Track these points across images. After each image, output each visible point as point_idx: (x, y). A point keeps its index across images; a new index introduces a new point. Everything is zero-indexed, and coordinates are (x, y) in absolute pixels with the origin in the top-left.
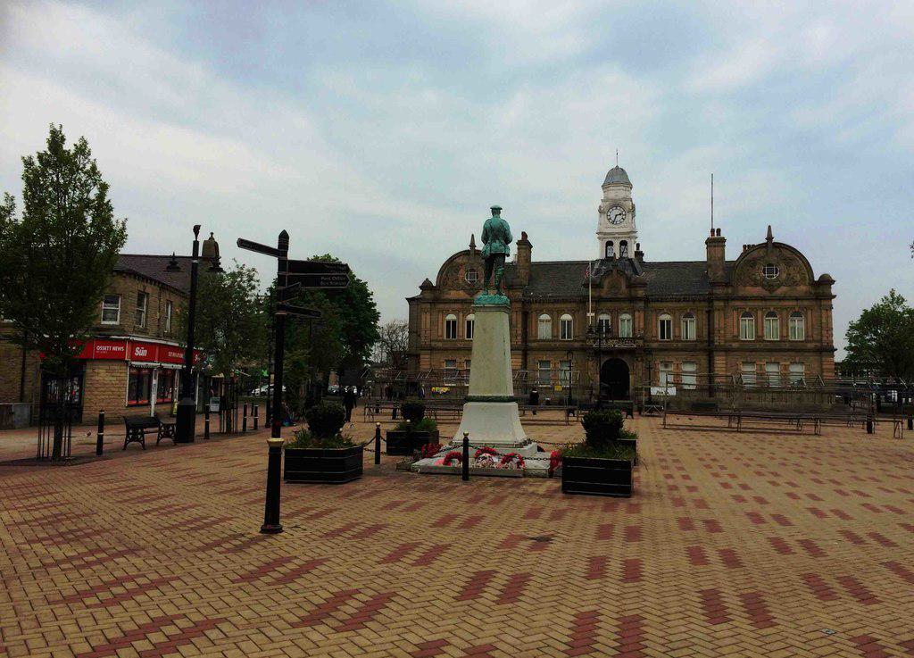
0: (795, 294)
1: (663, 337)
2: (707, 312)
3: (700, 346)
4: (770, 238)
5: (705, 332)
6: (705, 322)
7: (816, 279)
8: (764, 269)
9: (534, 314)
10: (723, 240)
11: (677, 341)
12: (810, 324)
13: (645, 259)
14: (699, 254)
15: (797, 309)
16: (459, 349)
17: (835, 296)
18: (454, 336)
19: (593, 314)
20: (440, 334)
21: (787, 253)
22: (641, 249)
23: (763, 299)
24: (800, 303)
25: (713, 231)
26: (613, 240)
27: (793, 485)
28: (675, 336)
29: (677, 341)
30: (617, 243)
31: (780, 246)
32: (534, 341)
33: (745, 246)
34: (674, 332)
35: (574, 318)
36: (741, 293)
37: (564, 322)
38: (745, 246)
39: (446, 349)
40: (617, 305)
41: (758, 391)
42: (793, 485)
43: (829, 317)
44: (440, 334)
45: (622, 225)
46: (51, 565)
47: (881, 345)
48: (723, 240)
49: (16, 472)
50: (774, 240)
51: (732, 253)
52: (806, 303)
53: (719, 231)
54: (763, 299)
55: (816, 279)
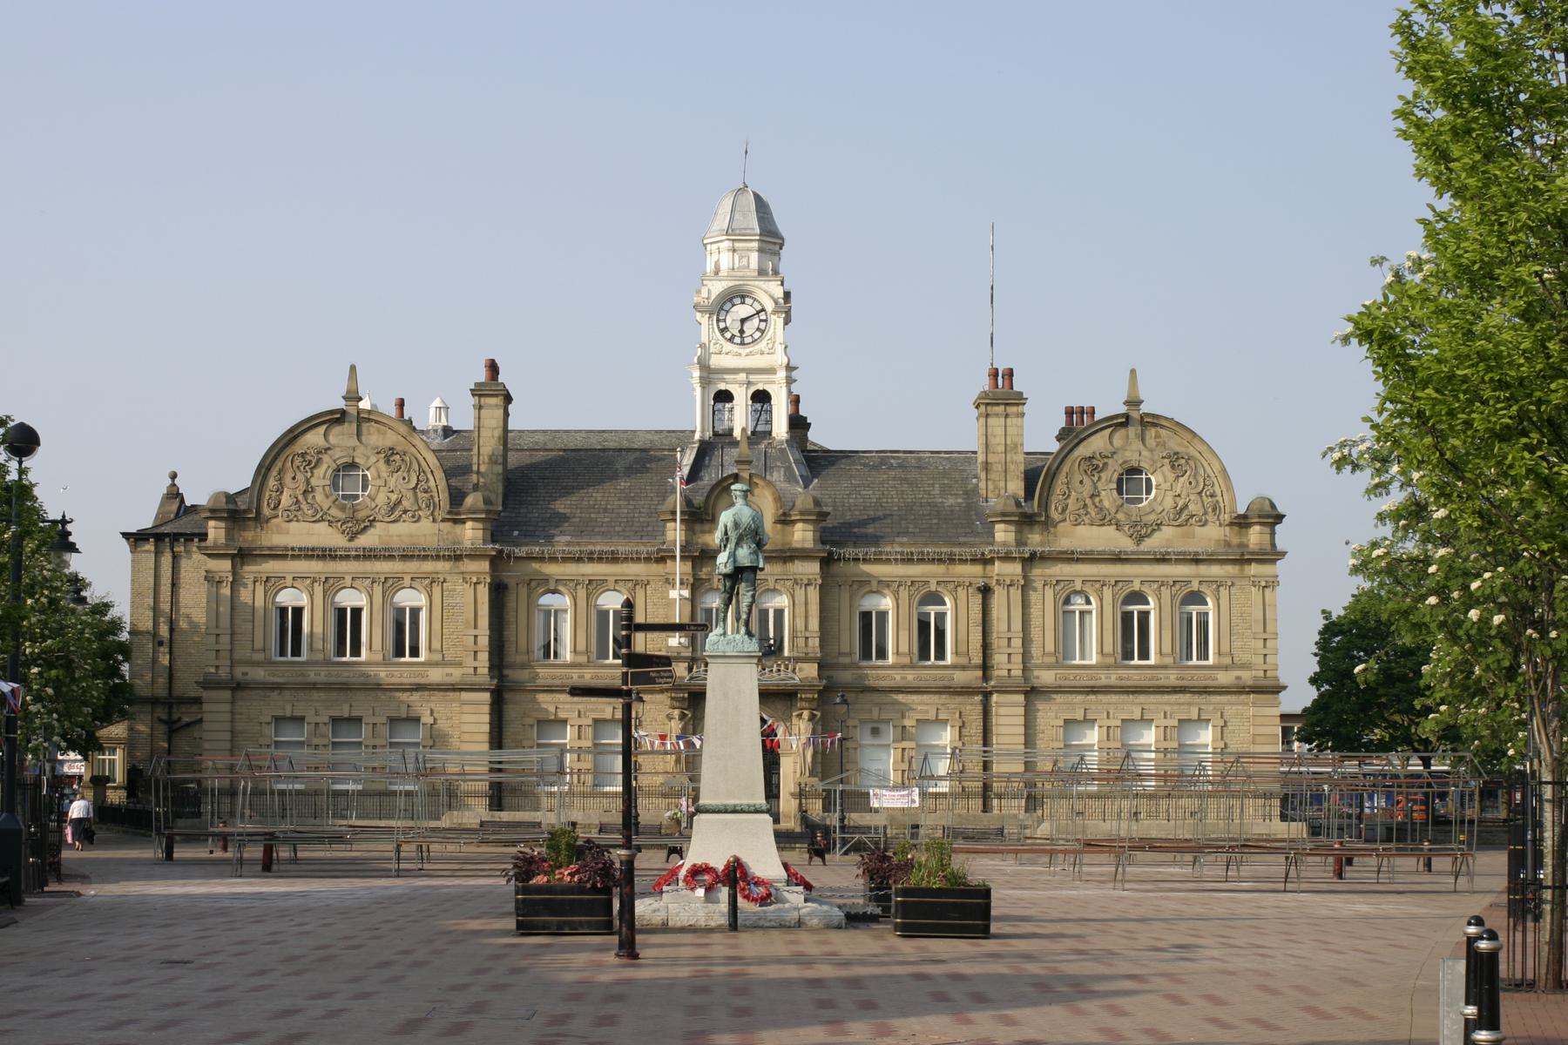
0: (1192, 547)
4: (1134, 403)
8: (365, 488)
9: (523, 591)
10: (1019, 399)
13: (813, 435)
16: (314, 687)
18: (296, 651)
19: (686, 593)
20: (259, 644)
23: (1118, 558)
24: (1203, 569)
27: (1218, 1002)
30: (741, 397)
33: (1070, 412)
36: (1064, 544)
39: (279, 687)
41: (1123, 422)
42: (1218, 1002)
44: (259, 644)
45: (756, 348)
46: (268, 851)
47: (1420, 693)
52: (1216, 570)
53: (1010, 374)
54: (1118, 558)
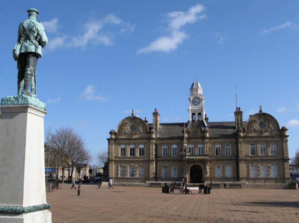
1: (217, 155)
2: (236, 143)
3: (233, 158)
5: (235, 152)
6: (235, 147)
7: (281, 128)
10: (241, 112)
11: (169, 157)
12: (279, 148)
14: (231, 118)
15: (253, 142)
17: (288, 136)
18: (143, 155)
20: (223, 153)
21: (268, 118)
22: (207, 117)
25: (237, 108)
26: (195, 113)
28: (222, 154)
29: (169, 157)
30: (197, 114)
31: (264, 114)
32: (160, 157)
34: (222, 153)
35: (145, 147)
37: (173, 149)
38: (250, 116)
40: (171, 141)
43: (286, 145)
48: (241, 112)
49: (256, 206)
50: (263, 112)
51: (246, 118)
53: (239, 108)
55: (281, 128)
